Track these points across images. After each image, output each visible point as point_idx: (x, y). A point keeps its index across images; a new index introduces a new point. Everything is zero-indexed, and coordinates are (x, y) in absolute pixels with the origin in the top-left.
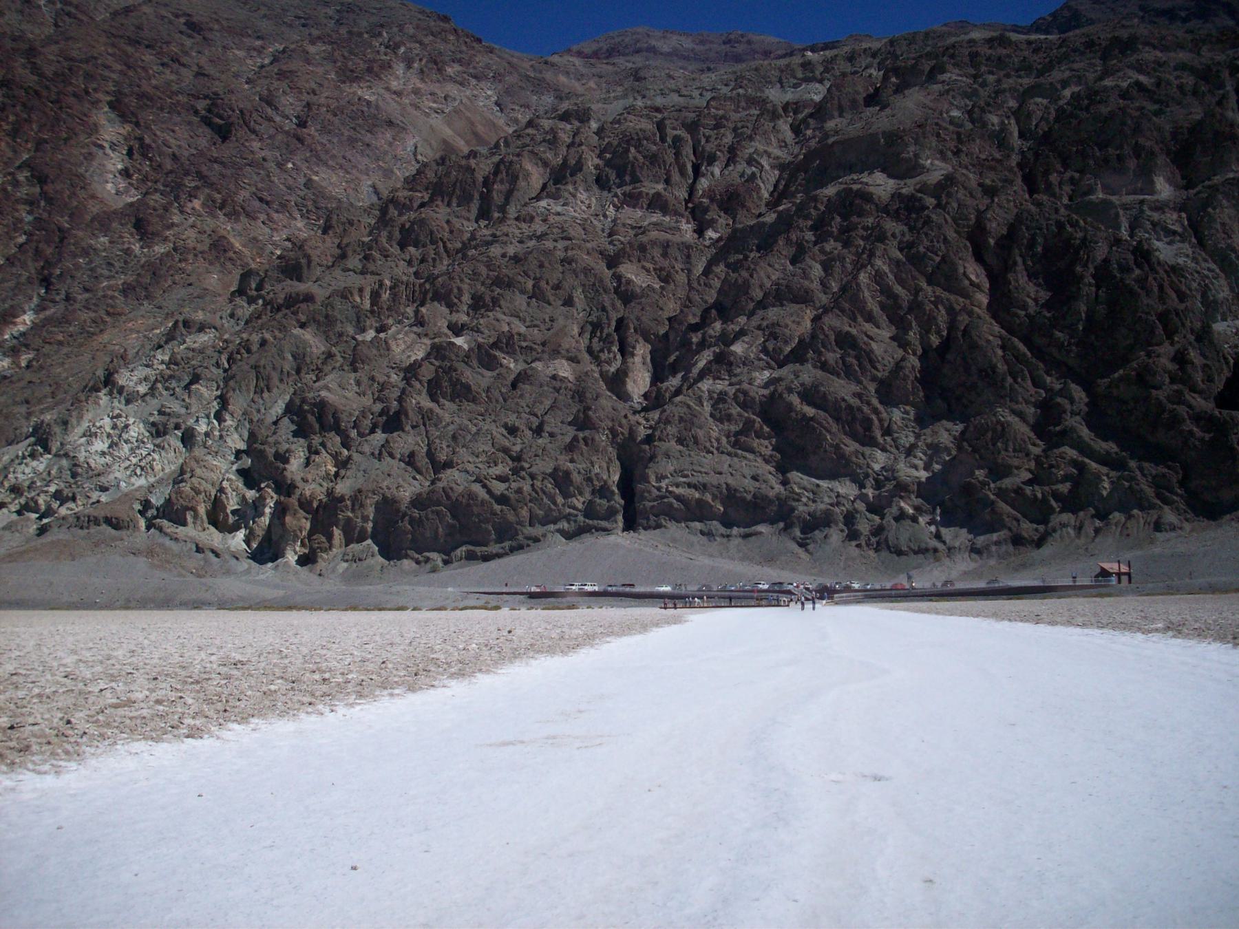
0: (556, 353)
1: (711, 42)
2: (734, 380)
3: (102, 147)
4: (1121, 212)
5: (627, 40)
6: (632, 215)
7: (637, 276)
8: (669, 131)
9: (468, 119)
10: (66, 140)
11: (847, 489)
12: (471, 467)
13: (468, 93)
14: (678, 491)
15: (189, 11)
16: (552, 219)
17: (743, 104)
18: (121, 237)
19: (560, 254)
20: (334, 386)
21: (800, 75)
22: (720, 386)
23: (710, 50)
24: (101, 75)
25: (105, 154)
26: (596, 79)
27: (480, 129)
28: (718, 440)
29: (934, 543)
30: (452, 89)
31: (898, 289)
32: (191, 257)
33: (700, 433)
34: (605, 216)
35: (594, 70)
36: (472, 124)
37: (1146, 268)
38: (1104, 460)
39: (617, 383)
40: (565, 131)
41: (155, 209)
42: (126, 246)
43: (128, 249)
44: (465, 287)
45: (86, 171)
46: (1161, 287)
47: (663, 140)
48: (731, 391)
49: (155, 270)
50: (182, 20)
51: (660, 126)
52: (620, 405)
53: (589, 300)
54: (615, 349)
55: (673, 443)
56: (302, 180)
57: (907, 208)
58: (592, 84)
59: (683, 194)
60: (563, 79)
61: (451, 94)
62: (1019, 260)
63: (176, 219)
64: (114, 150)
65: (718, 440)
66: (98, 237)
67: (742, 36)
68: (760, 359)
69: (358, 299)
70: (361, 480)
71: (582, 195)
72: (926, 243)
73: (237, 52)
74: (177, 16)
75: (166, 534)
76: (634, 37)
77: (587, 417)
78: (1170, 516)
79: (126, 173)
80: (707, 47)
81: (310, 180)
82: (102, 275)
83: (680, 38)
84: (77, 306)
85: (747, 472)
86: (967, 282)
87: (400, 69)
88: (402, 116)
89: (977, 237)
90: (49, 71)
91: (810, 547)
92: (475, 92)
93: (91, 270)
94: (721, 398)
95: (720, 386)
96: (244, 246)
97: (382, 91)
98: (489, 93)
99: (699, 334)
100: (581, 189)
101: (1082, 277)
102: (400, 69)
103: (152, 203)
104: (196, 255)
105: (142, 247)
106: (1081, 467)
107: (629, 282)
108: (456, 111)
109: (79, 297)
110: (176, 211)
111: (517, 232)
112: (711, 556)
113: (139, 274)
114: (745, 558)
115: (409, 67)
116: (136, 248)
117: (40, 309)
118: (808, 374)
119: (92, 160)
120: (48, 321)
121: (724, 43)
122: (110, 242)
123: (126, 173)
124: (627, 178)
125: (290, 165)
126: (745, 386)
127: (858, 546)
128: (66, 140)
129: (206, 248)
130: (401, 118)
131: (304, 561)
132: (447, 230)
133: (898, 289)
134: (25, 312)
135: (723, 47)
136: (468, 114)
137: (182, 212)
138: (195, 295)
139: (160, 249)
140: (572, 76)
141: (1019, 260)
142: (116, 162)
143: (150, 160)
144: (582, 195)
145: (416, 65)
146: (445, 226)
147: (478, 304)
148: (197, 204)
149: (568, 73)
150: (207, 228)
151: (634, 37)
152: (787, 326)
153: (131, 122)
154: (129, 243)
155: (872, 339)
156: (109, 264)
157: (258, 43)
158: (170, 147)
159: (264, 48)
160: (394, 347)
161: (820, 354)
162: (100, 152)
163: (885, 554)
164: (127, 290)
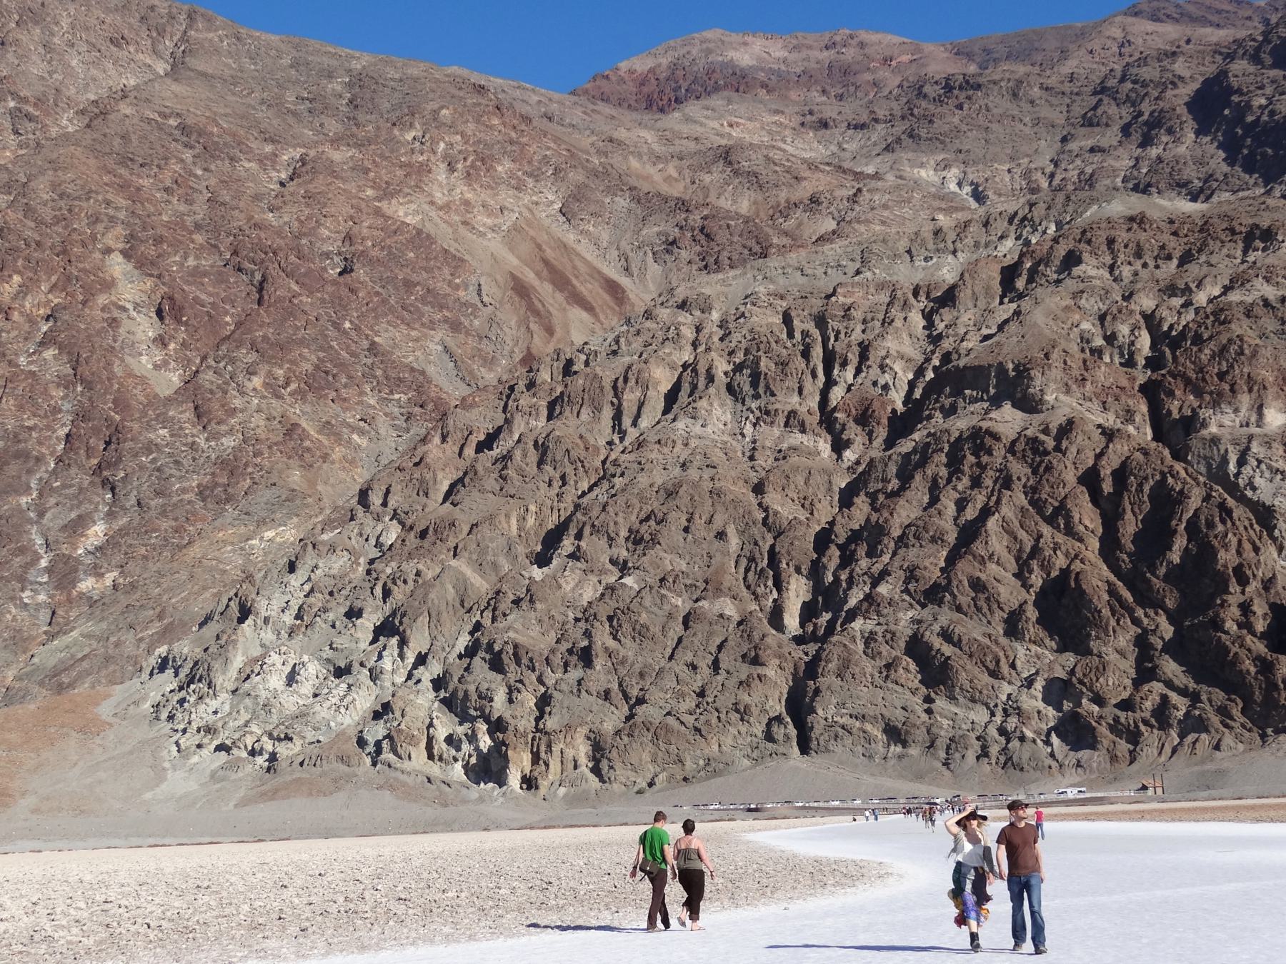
0: (719, 591)
1: (810, 47)
2: (882, 620)
3: (125, 309)
4: (1231, 448)
5: (694, 52)
6: (771, 435)
7: (782, 505)
8: (796, 322)
9: (533, 239)
10: (84, 303)
11: (980, 715)
12: (662, 703)
13: (527, 199)
14: (842, 721)
15: (179, 108)
16: (693, 443)
17: (872, 290)
18: (181, 428)
19: (707, 485)
20: (518, 626)
21: (931, 246)
22: (870, 625)
23: (807, 59)
24: (107, 215)
25: (129, 318)
26: (676, 162)
27: (549, 254)
28: (872, 676)
29: (1049, 761)
30: (506, 196)
31: (1022, 534)
32: (264, 448)
33: (857, 670)
34: (743, 435)
35: (671, 149)
36: (539, 247)
37: (1229, 524)
38: (1183, 692)
39: (776, 618)
40: (686, 321)
41: (212, 392)
42: (190, 440)
43: (193, 443)
44: (620, 519)
45: (115, 341)
46: (1240, 542)
47: (791, 335)
48: (879, 630)
49: (231, 466)
50: (173, 122)
51: (787, 319)
52: (781, 635)
53: (741, 533)
54: (770, 583)
55: (834, 678)
56: (365, 344)
57: (1031, 450)
58: (672, 171)
59: (813, 402)
60: (634, 163)
61: (507, 205)
62: (1128, 508)
63: (237, 402)
64: (139, 312)
65: (872, 676)
66: (156, 430)
67: (852, 37)
68: (903, 600)
69: (505, 526)
70: (567, 716)
71: (717, 411)
72: (1047, 488)
73: (247, 165)
74: (165, 116)
75: (396, 769)
76: (704, 46)
77: (757, 656)
78: (1228, 740)
79: (161, 341)
80: (804, 53)
81: (373, 344)
82: (171, 476)
83: (767, 43)
84: (153, 513)
85: (899, 704)
86: (1081, 528)
87: (441, 173)
88: (456, 240)
89: (1090, 479)
90: (47, 213)
91: (952, 767)
92: (534, 198)
93: (158, 470)
94: (869, 639)
95: (870, 625)
96: (319, 432)
97: (426, 207)
98: (551, 197)
99: (847, 571)
100: (715, 405)
101: (1175, 531)
102: (441, 173)
103: (207, 385)
104: (270, 447)
105: (207, 440)
106: (1164, 698)
107: (776, 513)
108: (515, 228)
109: (153, 503)
110: (235, 393)
111: (660, 457)
112: (873, 775)
113: (213, 474)
114: (901, 776)
115: (451, 168)
116: (201, 440)
117: (110, 515)
118: (946, 616)
119: (118, 327)
120: (123, 532)
121: (827, 48)
122: (172, 436)
123: (161, 341)
124: (761, 391)
125: (347, 325)
126: (892, 627)
127: (990, 764)
128: (84, 303)
129: (280, 438)
130: (456, 245)
131: (529, 783)
132: (582, 446)
133: (1022, 534)
134: (95, 523)
135: (826, 53)
136: (532, 233)
137: (243, 393)
138: (283, 497)
139: (229, 442)
140: (645, 158)
141: (1128, 508)
142: (144, 327)
143: (186, 324)
144: (717, 411)
145: (459, 166)
146: (579, 441)
147: (636, 539)
148: (257, 381)
149: (640, 156)
150: (275, 414)
151: (704, 46)
152: (926, 568)
153: (151, 275)
154: (193, 436)
155: (998, 581)
156: (177, 463)
157: (268, 148)
158: (203, 306)
159: (276, 156)
160: (564, 585)
161: (955, 597)
162: (124, 316)
163: (1011, 770)
164: (202, 493)
